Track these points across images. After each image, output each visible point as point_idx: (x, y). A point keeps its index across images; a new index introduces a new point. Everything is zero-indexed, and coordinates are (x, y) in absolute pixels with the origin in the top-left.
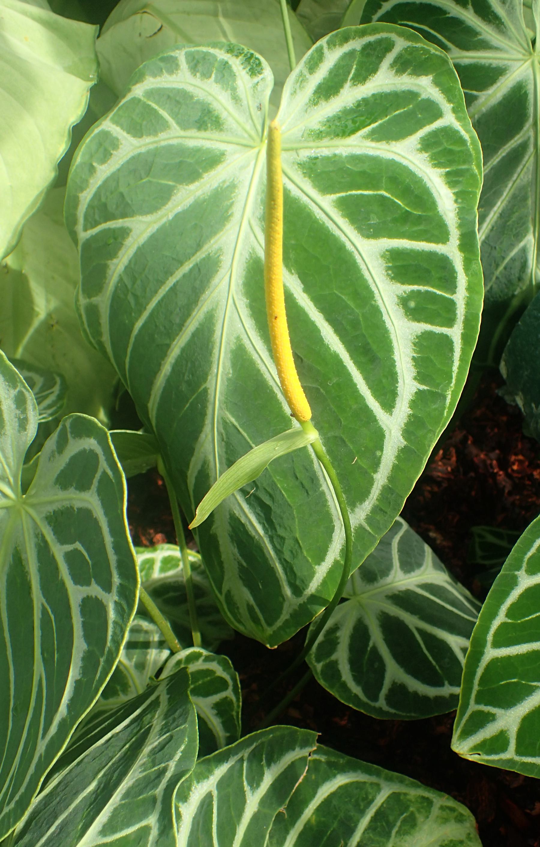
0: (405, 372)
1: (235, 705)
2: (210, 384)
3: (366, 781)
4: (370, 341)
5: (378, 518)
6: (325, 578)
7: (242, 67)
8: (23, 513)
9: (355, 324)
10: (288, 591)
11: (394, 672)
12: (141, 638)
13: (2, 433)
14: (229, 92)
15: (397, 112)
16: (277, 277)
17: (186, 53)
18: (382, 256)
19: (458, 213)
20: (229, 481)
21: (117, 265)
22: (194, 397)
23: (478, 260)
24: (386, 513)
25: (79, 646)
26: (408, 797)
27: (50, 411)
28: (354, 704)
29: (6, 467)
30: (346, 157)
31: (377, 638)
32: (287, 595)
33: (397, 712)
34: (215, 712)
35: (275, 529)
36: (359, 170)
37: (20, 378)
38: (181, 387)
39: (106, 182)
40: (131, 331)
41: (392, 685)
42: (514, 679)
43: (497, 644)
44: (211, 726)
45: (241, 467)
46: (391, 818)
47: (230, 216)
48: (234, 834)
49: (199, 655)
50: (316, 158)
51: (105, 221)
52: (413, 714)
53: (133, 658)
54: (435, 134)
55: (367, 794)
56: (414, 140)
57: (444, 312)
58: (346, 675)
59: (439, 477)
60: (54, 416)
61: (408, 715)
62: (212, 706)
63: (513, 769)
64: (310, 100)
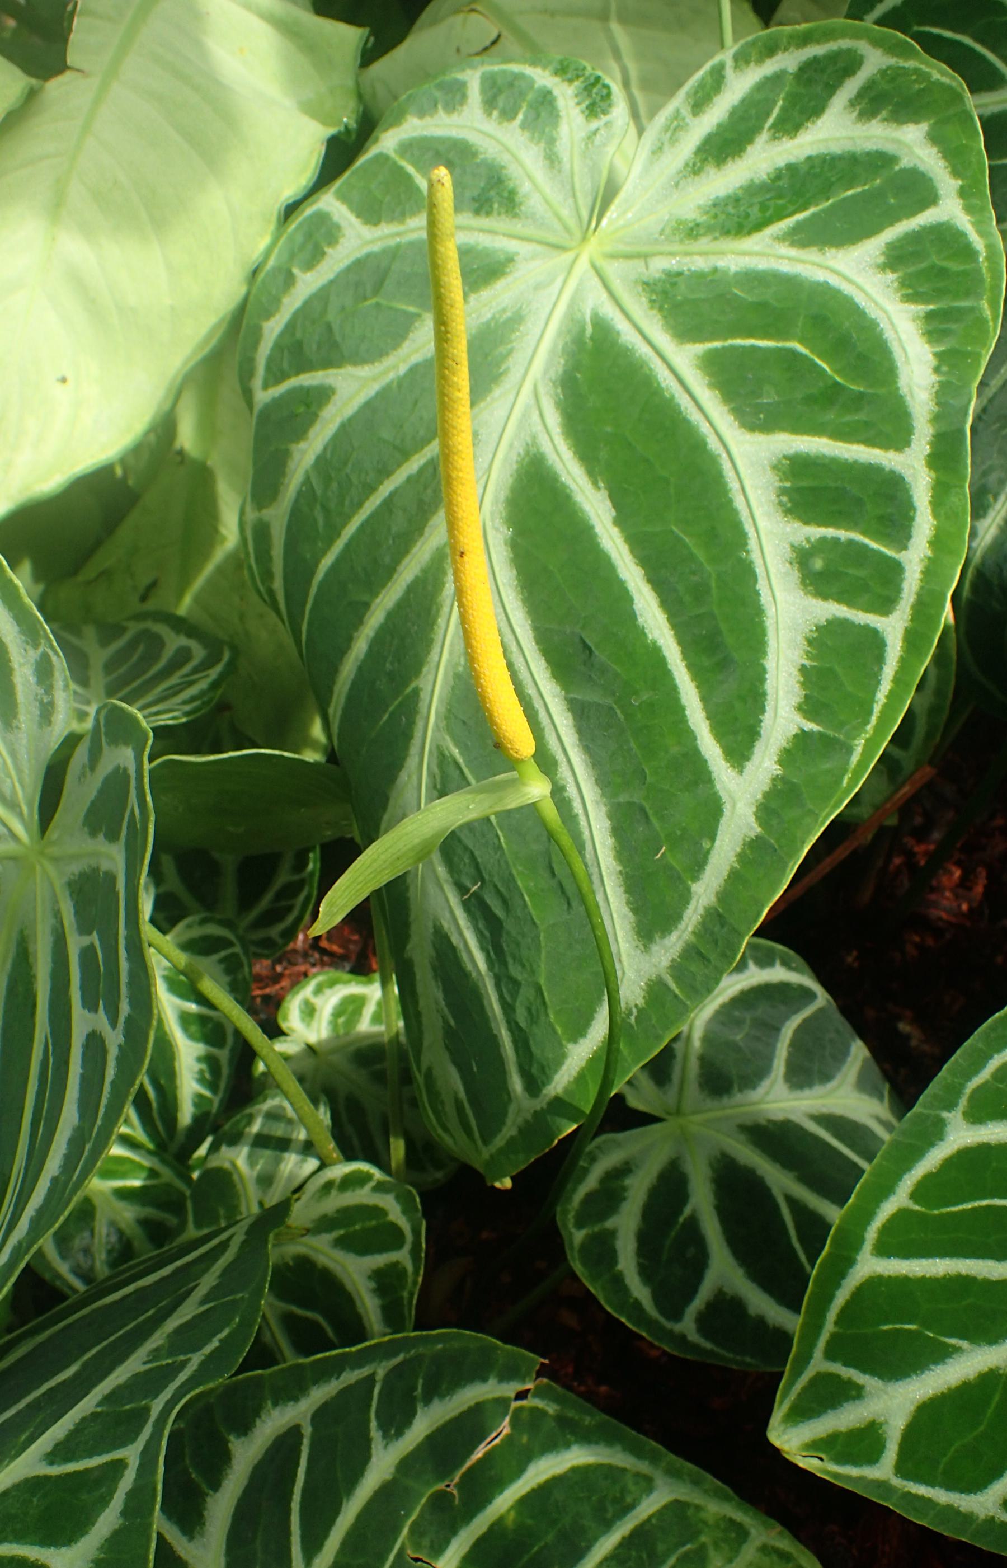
0: (781, 693)
1: (410, 1280)
2: (423, 682)
3: (628, 1467)
4: (723, 627)
5: (693, 968)
6: (583, 1069)
7: (576, 100)
8: (38, 867)
9: (700, 592)
10: (517, 1084)
11: (723, 1271)
12: (279, 1130)
13: (14, 725)
14: (542, 145)
15: (850, 193)
16: (461, 474)
17: (483, 74)
18: (775, 468)
19: (936, 392)
20: (383, 857)
21: (304, 453)
22: (396, 702)
23: (963, 487)
24: (709, 961)
25: (70, 1115)
26: (703, 1515)
27: (187, 708)
28: (629, 1318)
29: (17, 784)
30: (736, 274)
31: (702, 1200)
32: (515, 1091)
33: (717, 1350)
34: (372, 1285)
35: (505, 964)
36: (754, 299)
37: (45, 630)
38: (378, 683)
39: (307, 304)
40: (312, 573)
41: (716, 1296)
42: (910, 1323)
43: (883, 1250)
44: (361, 1311)
45: (407, 834)
46: (661, 1547)
47: (501, 374)
48: (336, 1511)
49: (368, 1177)
50: (679, 274)
51: (298, 373)
52: (748, 1359)
53: (257, 1163)
54: (915, 237)
55: (624, 1491)
56: (874, 247)
57: (878, 584)
58: (627, 1261)
59: (940, 919)
60: (191, 718)
61: (738, 1358)
62: (370, 1273)
63: (885, 1500)
64: (687, 165)
